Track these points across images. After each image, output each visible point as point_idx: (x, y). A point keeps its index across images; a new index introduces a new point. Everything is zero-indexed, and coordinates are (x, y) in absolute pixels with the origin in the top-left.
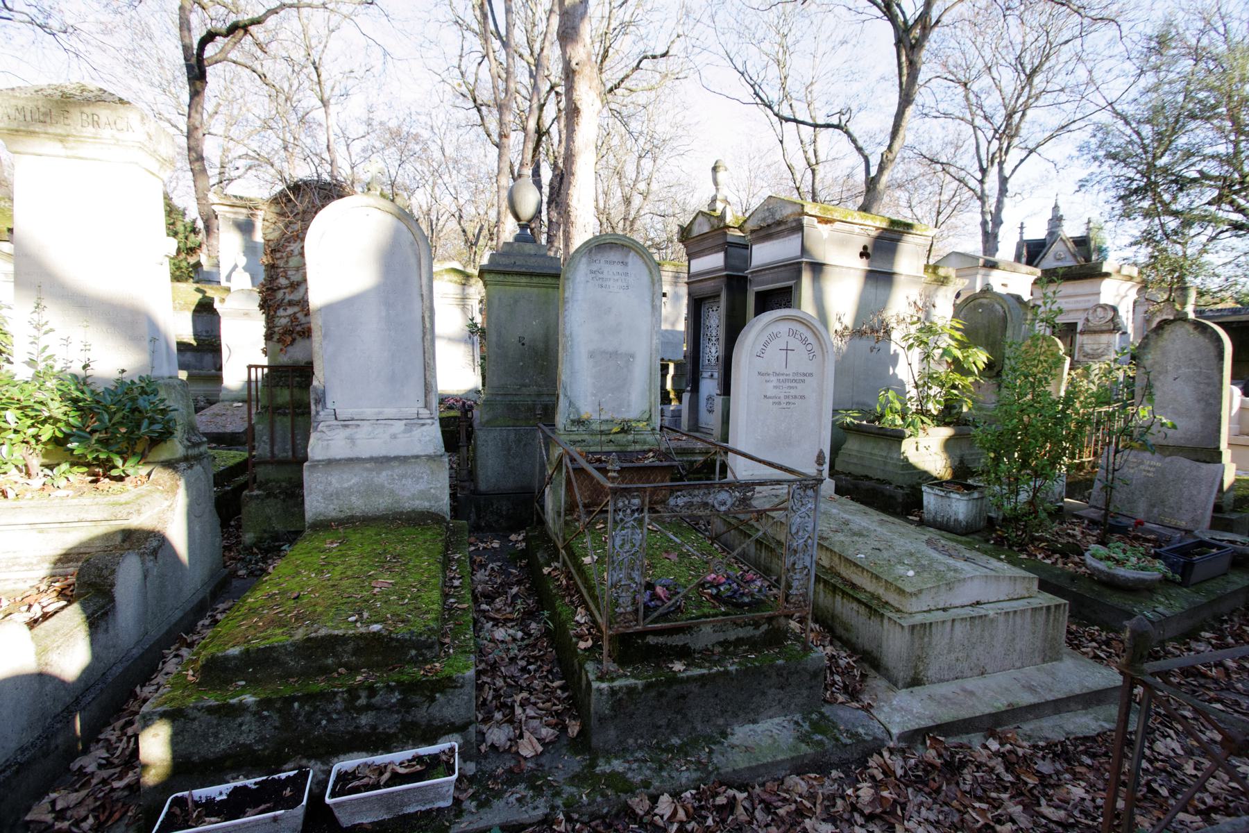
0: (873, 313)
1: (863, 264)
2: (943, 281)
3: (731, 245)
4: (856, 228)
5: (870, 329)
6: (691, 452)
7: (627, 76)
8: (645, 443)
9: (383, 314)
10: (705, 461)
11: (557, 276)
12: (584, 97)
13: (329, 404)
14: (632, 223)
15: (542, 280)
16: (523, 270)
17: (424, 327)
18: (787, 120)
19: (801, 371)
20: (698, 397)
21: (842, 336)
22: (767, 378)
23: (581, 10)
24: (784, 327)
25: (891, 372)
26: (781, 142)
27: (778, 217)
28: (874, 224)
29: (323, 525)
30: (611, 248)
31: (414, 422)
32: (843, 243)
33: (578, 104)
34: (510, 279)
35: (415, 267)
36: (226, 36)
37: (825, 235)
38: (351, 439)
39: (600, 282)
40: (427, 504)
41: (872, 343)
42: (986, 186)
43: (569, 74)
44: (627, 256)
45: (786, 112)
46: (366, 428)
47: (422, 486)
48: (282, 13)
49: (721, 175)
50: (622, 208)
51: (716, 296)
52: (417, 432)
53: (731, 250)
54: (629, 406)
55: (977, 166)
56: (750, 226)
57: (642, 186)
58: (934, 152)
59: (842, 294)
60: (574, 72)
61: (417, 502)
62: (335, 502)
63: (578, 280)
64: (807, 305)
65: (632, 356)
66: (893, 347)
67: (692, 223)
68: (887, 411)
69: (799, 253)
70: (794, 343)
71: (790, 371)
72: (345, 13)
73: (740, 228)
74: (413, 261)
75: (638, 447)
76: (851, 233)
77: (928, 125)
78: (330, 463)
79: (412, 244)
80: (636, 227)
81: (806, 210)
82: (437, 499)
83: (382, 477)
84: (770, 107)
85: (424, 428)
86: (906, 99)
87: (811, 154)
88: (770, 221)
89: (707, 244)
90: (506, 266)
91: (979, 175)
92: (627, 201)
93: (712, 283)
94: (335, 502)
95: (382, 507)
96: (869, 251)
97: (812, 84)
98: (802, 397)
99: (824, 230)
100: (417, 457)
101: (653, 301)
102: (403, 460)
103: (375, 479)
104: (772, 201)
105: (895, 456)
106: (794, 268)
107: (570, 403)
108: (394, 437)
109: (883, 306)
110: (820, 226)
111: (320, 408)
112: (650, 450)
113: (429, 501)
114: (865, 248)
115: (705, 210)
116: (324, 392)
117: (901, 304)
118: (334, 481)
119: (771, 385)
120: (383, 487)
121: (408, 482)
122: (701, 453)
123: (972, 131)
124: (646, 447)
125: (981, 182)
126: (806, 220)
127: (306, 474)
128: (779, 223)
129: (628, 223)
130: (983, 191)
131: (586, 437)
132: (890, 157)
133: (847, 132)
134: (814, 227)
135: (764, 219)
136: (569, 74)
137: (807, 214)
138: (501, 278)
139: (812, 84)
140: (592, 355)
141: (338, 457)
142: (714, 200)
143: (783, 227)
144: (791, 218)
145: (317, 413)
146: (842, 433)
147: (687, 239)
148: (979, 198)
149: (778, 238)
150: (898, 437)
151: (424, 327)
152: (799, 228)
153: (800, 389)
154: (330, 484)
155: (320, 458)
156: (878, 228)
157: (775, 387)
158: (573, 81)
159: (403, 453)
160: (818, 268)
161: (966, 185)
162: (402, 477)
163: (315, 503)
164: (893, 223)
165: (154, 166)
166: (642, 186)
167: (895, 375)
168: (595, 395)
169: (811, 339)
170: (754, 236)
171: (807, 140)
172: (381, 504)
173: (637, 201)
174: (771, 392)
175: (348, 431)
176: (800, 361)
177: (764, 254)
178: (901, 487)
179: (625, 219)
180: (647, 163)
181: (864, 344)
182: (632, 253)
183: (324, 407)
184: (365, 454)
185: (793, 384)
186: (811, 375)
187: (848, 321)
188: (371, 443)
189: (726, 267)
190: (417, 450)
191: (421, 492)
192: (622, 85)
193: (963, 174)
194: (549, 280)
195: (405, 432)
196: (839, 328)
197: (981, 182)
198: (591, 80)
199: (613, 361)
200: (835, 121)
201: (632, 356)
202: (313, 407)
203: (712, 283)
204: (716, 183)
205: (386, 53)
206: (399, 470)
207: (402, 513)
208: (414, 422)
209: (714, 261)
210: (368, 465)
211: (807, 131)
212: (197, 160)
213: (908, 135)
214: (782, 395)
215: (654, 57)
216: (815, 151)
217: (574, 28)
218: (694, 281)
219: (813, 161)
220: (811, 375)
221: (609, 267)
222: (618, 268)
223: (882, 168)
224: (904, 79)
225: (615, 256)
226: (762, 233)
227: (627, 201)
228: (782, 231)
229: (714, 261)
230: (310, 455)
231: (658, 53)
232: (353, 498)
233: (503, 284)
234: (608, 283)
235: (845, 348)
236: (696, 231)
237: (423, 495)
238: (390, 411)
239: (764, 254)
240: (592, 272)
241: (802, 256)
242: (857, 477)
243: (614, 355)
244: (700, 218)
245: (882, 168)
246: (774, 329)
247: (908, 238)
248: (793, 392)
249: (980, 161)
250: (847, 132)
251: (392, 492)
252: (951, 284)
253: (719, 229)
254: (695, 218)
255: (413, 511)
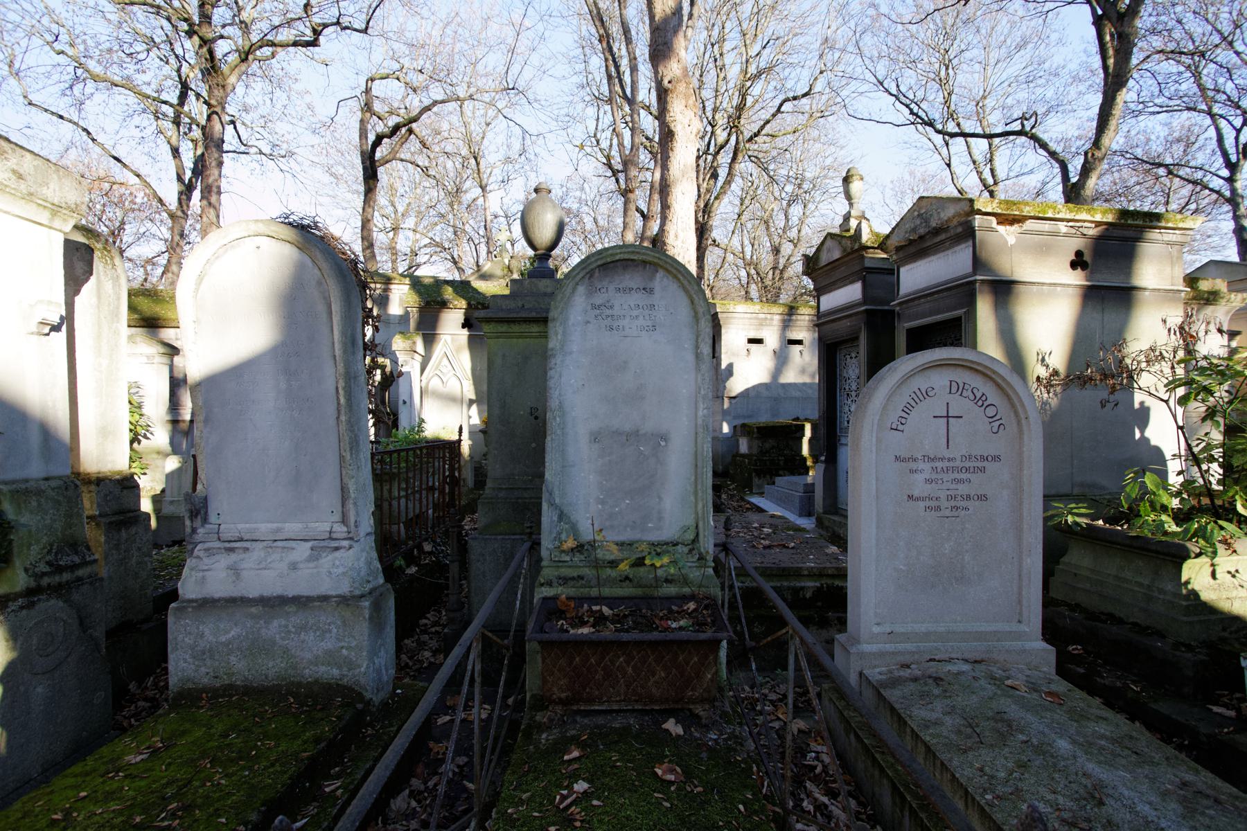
0: (1103, 347)
1: (1077, 278)
2: (1211, 298)
3: (870, 270)
4: (1062, 227)
5: (1099, 372)
6: (797, 573)
7: (768, 122)
8: (685, 581)
9: (283, 386)
10: (819, 590)
11: (544, 321)
12: (679, 117)
13: (213, 518)
14: (782, 272)
15: (524, 328)
16: (534, 314)
17: (339, 404)
18: (953, 135)
19: (977, 452)
20: (836, 470)
21: (1049, 386)
22: (913, 465)
23: (674, 22)
24: (940, 380)
25: (1138, 435)
26: (949, 165)
27: (934, 223)
28: (1094, 217)
29: (190, 697)
30: (625, 268)
31: (324, 545)
32: (1043, 250)
33: (672, 126)
34: (516, 328)
35: (324, 316)
36: (390, 137)
37: (1011, 240)
38: (235, 570)
39: (608, 322)
40: (335, 672)
41: (1104, 394)
42: (1238, 185)
43: (663, 94)
44: (652, 278)
45: (952, 127)
46: (258, 551)
47: (328, 644)
48: (435, 109)
49: (855, 186)
50: (771, 258)
51: (853, 339)
52: (327, 560)
53: (870, 277)
54: (660, 519)
55: (1220, 161)
56: (893, 242)
57: (793, 234)
58: (1154, 154)
59: (1048, 326)
60: (666, 91)
61: (323, 669)
62: (209, 662)
63: (572, 320)
64: (988, 342)
65: (665, 437)
66: (1138, 397)
67: (819, 250)
68: (1144, 507)
69: (969, 269)
70: (959, 405)
71: (957, 451)
72: (488, 100)
73: (882, 246)
74: (321, 308)
75: (672, 590)
76: (1055, 234)
77: (1142, 125)
78: (207, 604)
79: (319, 283)
80: (786, 275)
81: (977, 206)
82: (351, 665)
83: (274, 628)
84: (930, 124)
85: (337, 554)
86: (1115, 81)
87: (987, 175)
88: (922, 231)
89: (837, 274)
90: (509, 311)
91: (1225, 173)
92: (776, 251)
93: (847, 323)
94: (209, 662)
95: (271, 674)
96: (1087, 258)
97: (984, 97)
98: (982, 498)
99: (1009, 234)
100: (325, 598)
101: (697, 347)
102: (302, 602)
103: (263, 631)
104: (924, 203)
105: (1169, 587)
106: (963, 292)
107: (562, 516)
108: (294, 566)
109: (1119, 341)
110: (1001, 229)
111: (198, 522)
112: (692, 597)
113: (340, 668)
114: (1079, 254)
115: (837, 231)
116: (206, 498)
117: (1150, 329)
118: (207, 632)
119: (919, 477)
120: (274, 643)
121: (310, 637)
122: (812, 575)
123: (1208, 121)
124: (686, 590)
125: (1230, 180)
126: (978, 220)
127: (171, 620)
128: (937, 231)
129: (778, 272)
130: (1233, 191)
131: (586, 571)
132: (1098, 154)
133: (1034, 138)
134: (992, 230)
135: (914, 230)
136: (663, 94)
137: (980, 212)
138: (503, 328)
139: (984, 97)
140: (595, 438)
141: (217, 596)
142: (847, 218)
143: (943, 236)
144: (955, 222)
145: (194, 530)
146: (1058, 541)
147: (814, 270)
148: (1228, 201)
149: (935, 253)
150: (1179, 556)
151: (339, 404)
152: (967, 233)
153: (977, 483)
154: (202, 636)
155: (193, 596)
156: (1098, 224)
157: (927, 481)
158: (665, 102)
159: (306, 593)
160: (1004, 289)
161: (1206, 187)
162: (303, 628)
163: (182, 664)
164: (1124, 213)
165: (44, 217)
166: (793, 234)
167: (1145, 440)
168: (603, 502)
169: (993, 396)
170: (901, 254)
171: (979, 157)
172: (271, 669)
173: (787, 249)
174: (919, 487)
175: (233, 557)
176: (973, 432)
177: (915, 277)
178: (1189, 648)
179: (774, 268)
180: (796, 210)
181: (1090, 397)
182: (660, 274)
183: (205, 520)
184: (253, 593)
185: (964, 476)
186: (996, 458)
187: (1058, 361)
188: (263, 575)
189: (866, 298)
190: (325, 587)
191: (328, 653)
192: (763, 132)
193: (1199, 175)
194: (535, 328)
195: (311, 559)
196: (1042, 372)
197: (1230, 180)
198: (687, 97)
199: (634, 448)
200: (1016, 126)
201: (665, 437)
202: (188, 523)
203: (847, 323)
204: (848, 197)
205: (525, 132)
206: (296, 618)
207: (299, 684)
208: (324, 545)
209: (851, 293)
210: (253, 610)
211: (980, 145)
212: (368, 248)
213: (1114, 140)
214: (943, 495)
215: (795, 98)
216: (992, 171)
217: (665, 43)
218: (822, 322)
219: (990, 181)
220: (996, 458)
221: (623, 298)
222: (636, 298)
223: (1086, 171)
224: (1111, 61)
225: (632, 280)
226: (912, 250)
227: (776, 251)
228: (942, 242)
229: (851, 293)
230: (180, 592)
231: (799, 93)
232: (233, 659)
233: (507, 335)
234: (621, 323)
235: (1054, 402)
236: (825, 259)
237: (331, 657)
238: (293, 528)
239: (915, 277)
240: (594, 307)
241: (975, 272)
242: (1092, 616)
243: (634, 436)
244: (829, 243)
245: (1086, 171)
246: (921, 383)
247: (1154, 234)
248: (963, 489)
249: (1225, 154)
250: (1034, 138)
251: (286, 651)
252: (1223, 302)
253: (854, 251)
254: (822, 243)
255: (316, 681)
